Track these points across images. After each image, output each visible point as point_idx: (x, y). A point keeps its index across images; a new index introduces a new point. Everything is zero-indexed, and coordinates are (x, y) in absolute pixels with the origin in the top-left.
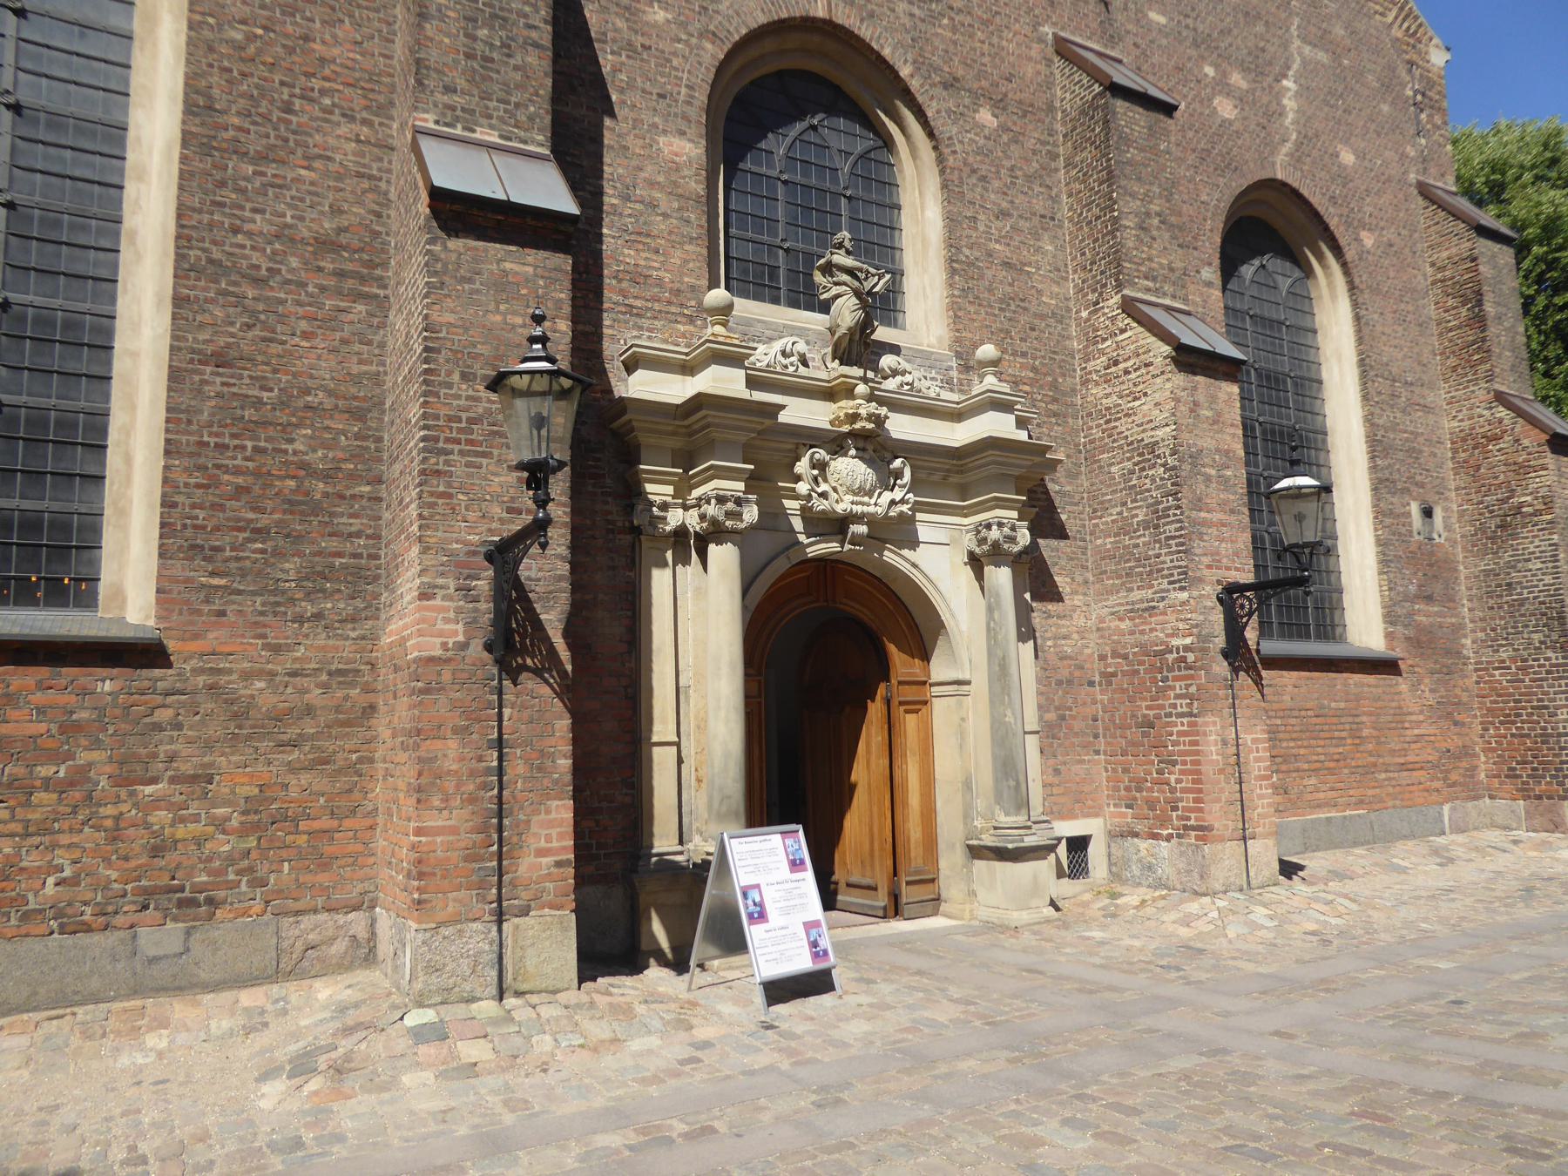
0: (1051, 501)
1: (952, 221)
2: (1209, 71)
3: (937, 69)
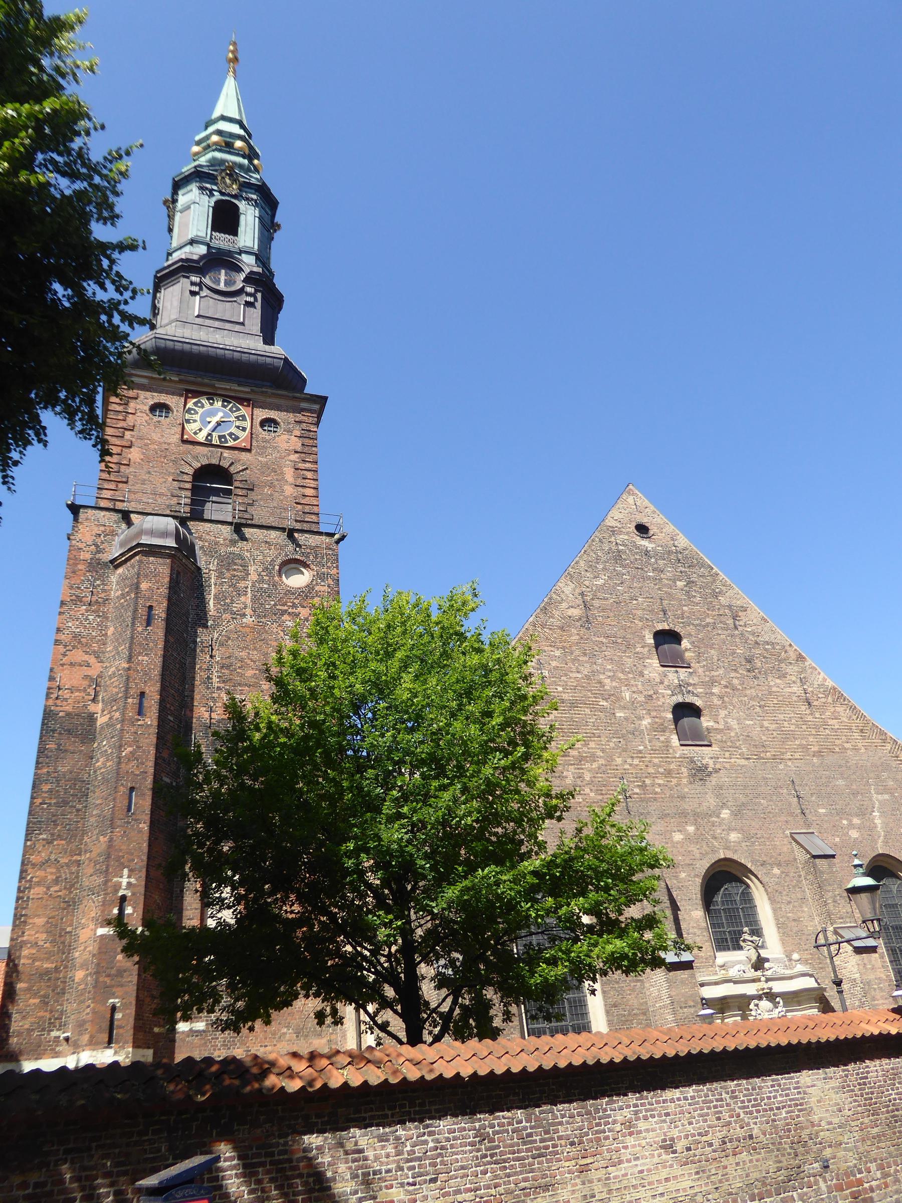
0: (827, 999)
1: (775, 910)
2: (845, 822)
3: (758, 861)
